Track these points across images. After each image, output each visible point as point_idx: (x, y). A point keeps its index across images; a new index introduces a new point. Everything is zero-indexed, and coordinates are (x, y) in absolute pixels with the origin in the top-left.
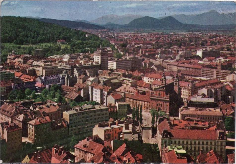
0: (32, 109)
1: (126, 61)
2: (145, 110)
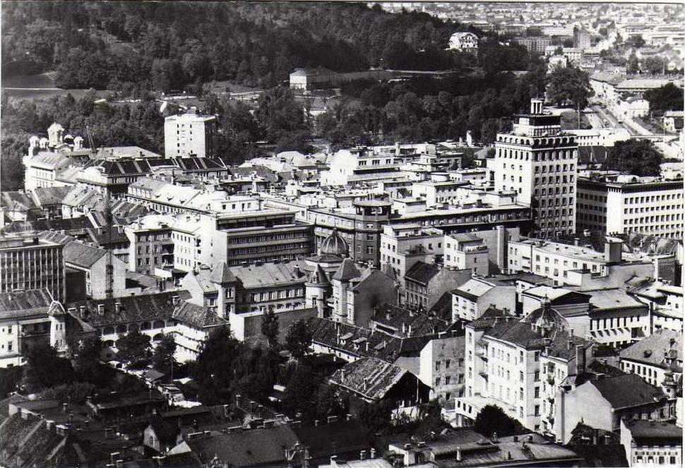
0: (155, 445)
2: (163, 265)
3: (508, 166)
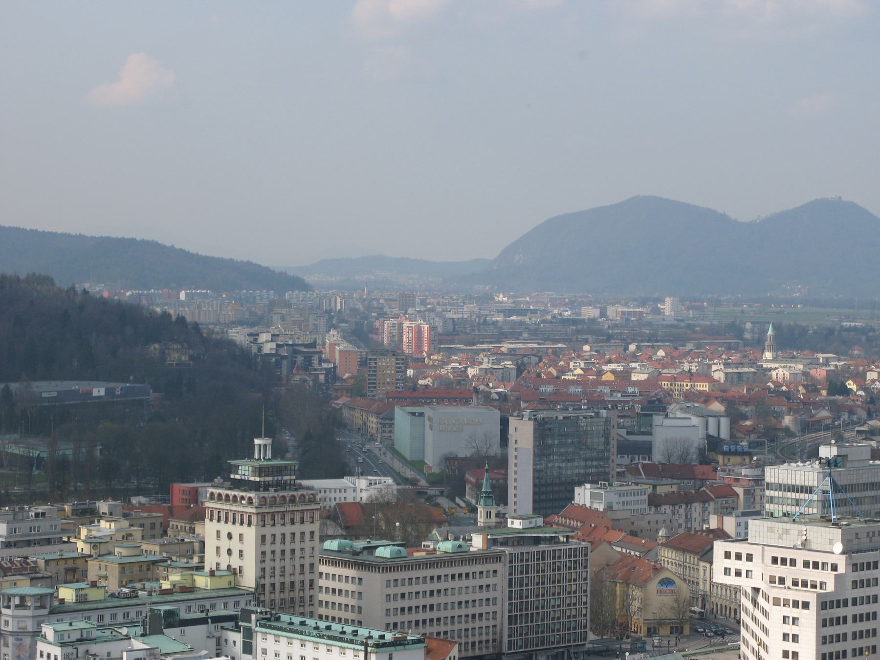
1: (462, 562)
3: (224, 535)
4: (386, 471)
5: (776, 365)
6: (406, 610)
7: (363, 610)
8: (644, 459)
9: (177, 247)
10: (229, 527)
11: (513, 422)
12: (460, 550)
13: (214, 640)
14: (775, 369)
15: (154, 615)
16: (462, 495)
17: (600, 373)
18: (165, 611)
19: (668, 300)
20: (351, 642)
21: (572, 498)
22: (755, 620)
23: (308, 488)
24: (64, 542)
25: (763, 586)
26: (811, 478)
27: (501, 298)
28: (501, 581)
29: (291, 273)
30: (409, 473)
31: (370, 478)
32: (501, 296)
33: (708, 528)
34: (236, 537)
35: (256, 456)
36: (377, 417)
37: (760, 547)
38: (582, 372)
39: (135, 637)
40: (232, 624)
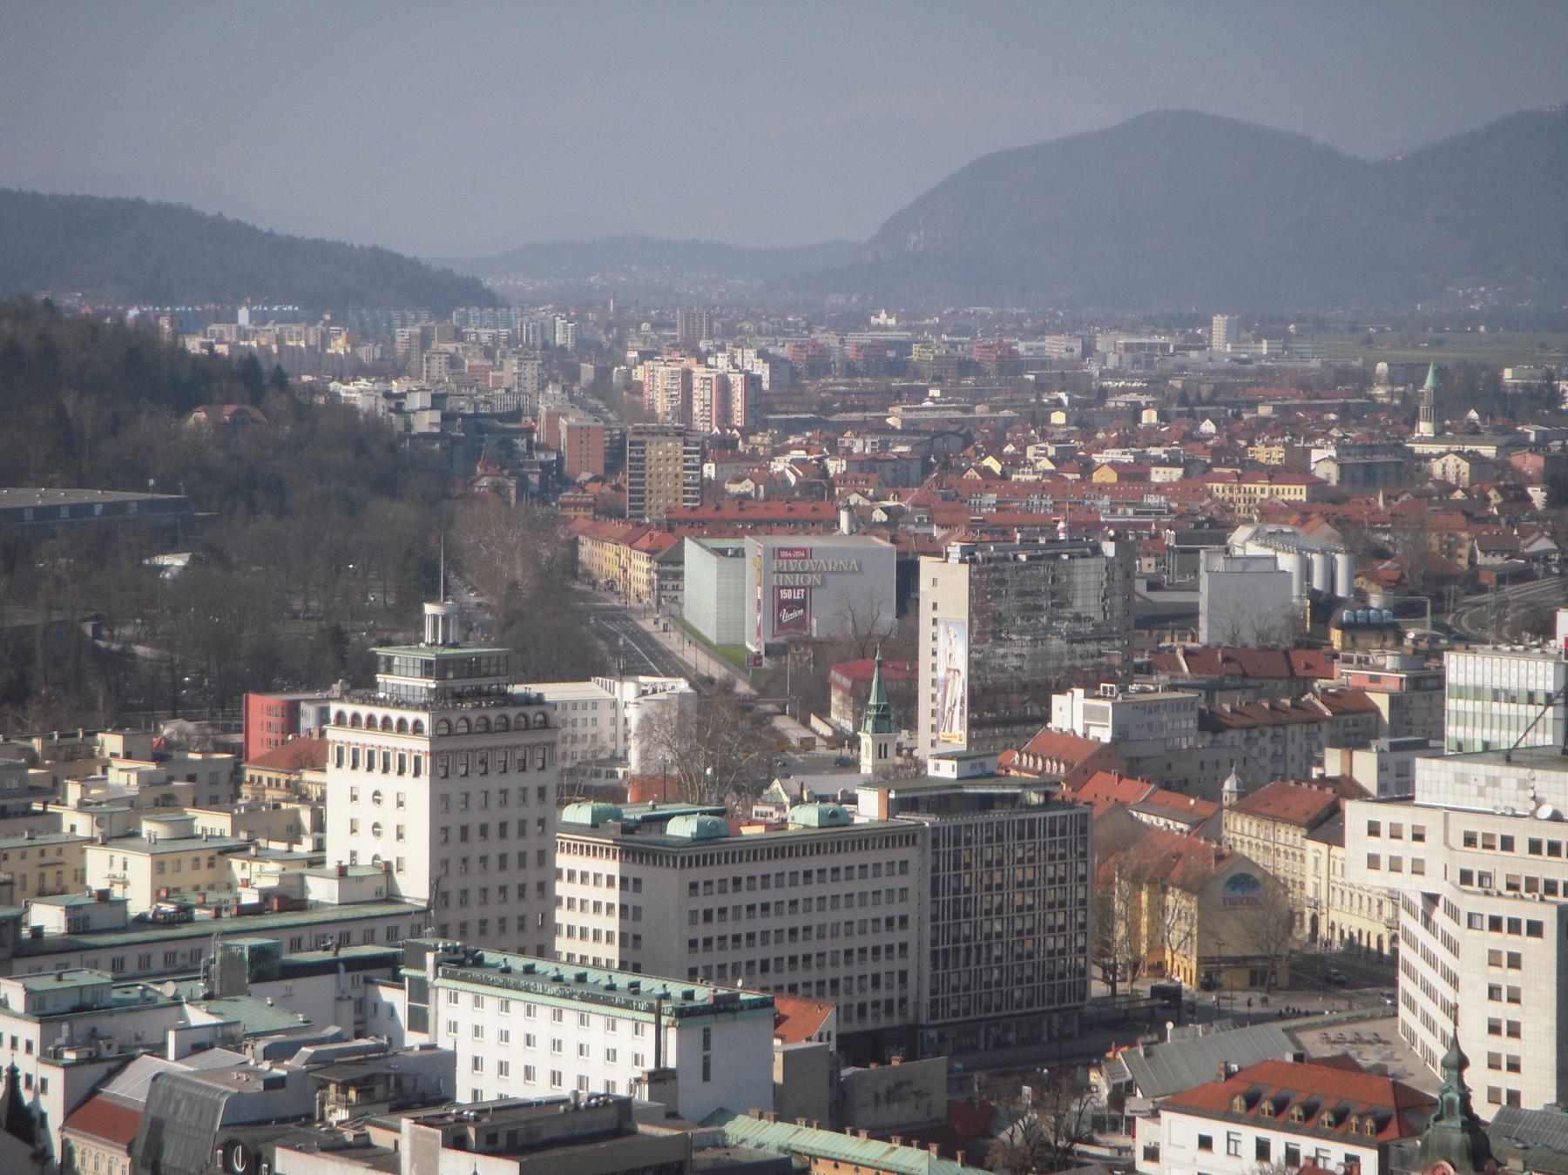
1: (839, 846)
4: (670, 666)
5: (1442, 448)
6: (883, 950)
7: (644, 942)
8: (1182, 638)
9: (230, 216)
10: (376, 780)
11: (927, 565)
12: (834, 821)
13: (351, 1004)
14: (1440, 456)
15: (231, 961)
16: (824, 713)
17: (1088, 468)
18: (252, 949)
19: (1219, 322)
20: (627, 1006)
21: (1046, 718)
22: (1432, 961)
23: (527, 701)
24: (37, 813)
25: (1446, 889)
26: (1541, 673)
27: (883, 318)
28: (916, 882)
29: (461, 271)
30: (717, 671)
31: (642, 679)
32: (883, 315)
33: (1322, 776)
34: (389, 799)
35: (428, 638)
36: (650, 559)
37: (1440, 814)
38: (1050, 466)
39: (190, 1001)
40: (387, 971)
